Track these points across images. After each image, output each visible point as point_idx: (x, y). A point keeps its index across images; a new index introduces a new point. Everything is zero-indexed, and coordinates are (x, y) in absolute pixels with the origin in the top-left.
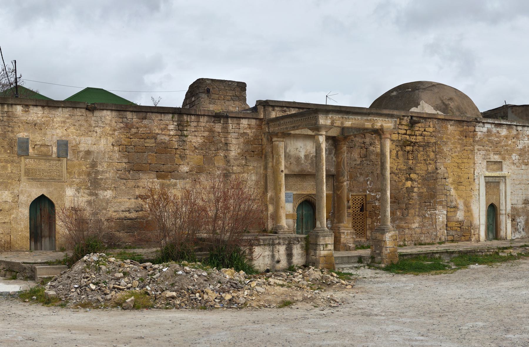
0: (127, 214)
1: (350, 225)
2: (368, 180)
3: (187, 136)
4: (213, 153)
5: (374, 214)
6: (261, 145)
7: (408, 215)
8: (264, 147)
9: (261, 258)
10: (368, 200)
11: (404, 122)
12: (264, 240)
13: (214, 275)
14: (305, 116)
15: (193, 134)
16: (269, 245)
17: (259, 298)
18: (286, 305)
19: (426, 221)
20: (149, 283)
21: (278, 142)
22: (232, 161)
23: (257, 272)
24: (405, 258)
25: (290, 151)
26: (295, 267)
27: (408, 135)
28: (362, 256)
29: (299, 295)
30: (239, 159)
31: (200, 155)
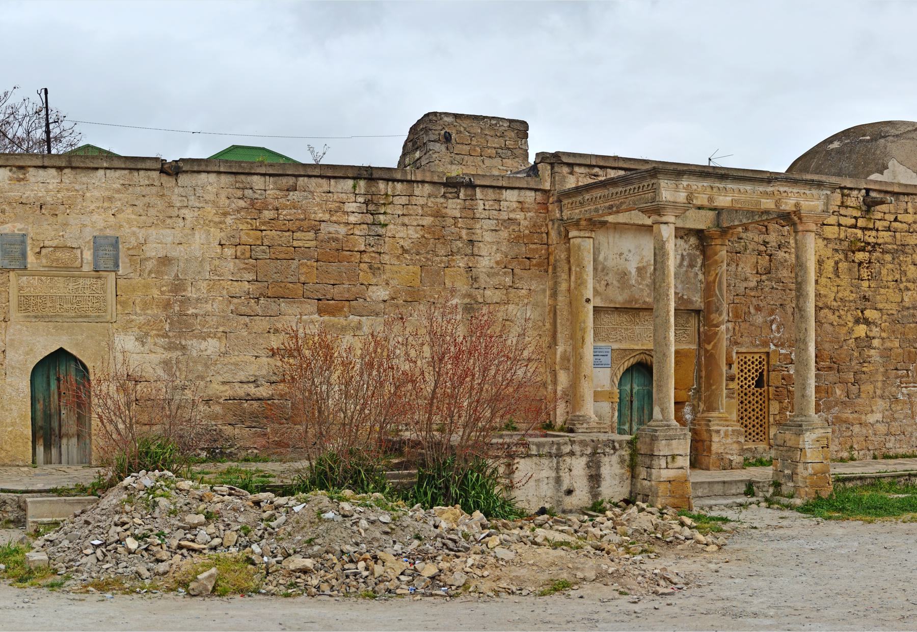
0: (252, 389)
1: (734, 416)
2: (772, 322)
3: (386, 225)
4: (441, 262)
5: (785, 392)
6: (547, 244)
7: (859, 396)
8: (552, 248)
9: (532, 483)
10: (772, 362)
11: (850, 202)
12: (539, 445)
13: (407, 521)
14: (632, 184)
15: (400, 220)
16: (550, 455)
17: (497, 572)
18: (556, 590)
19: (899, 408)
20: (262, 537)
21: (579, 240)
22: (483, 278)
23: (521, 514)
24: (849, 485)
25: (605, 259)
26: (604, 504)
27: (861, 228)
28: (754, 482)
29: (589, 566)
30: (498, 274)
31: (414, 264)
